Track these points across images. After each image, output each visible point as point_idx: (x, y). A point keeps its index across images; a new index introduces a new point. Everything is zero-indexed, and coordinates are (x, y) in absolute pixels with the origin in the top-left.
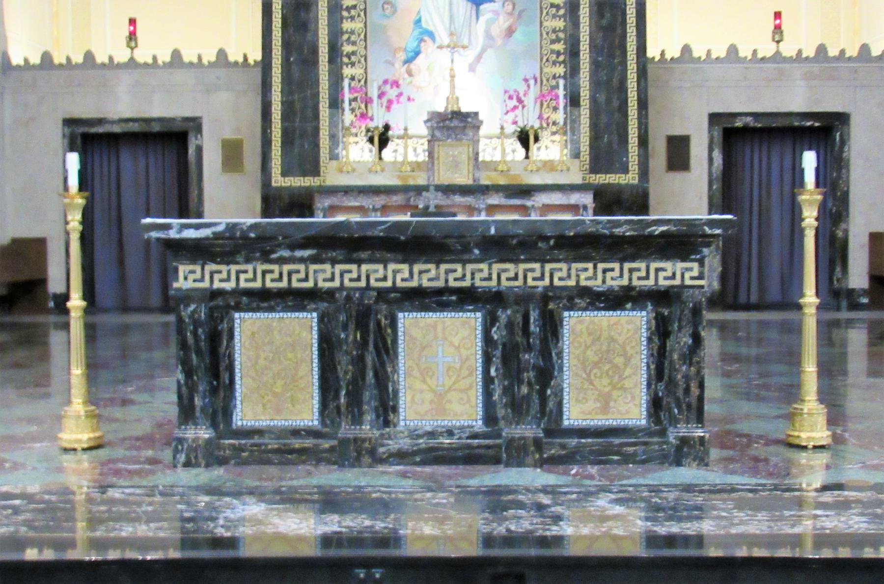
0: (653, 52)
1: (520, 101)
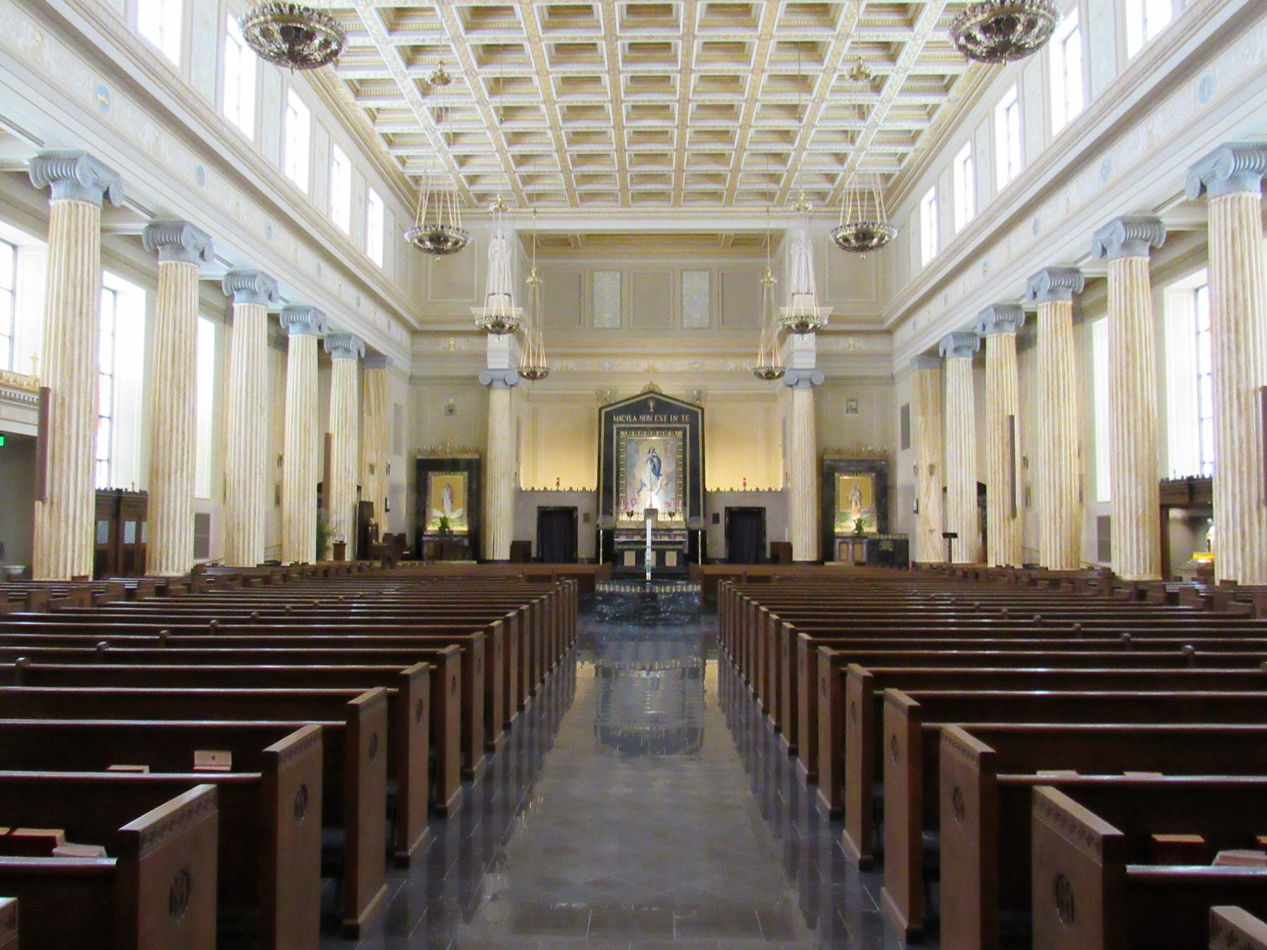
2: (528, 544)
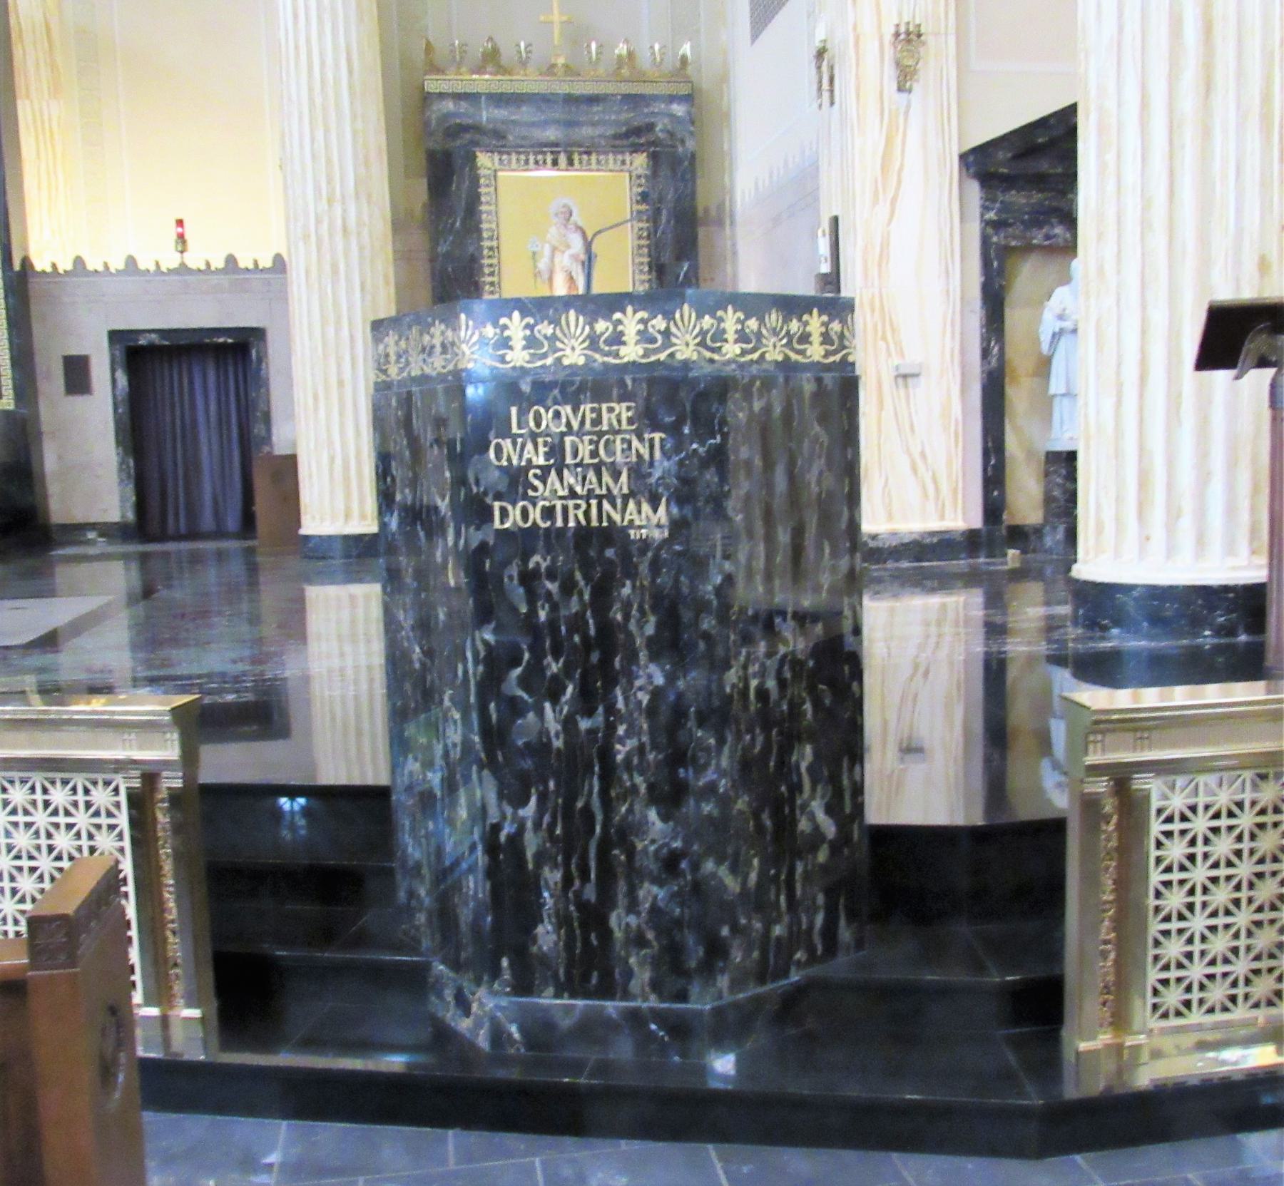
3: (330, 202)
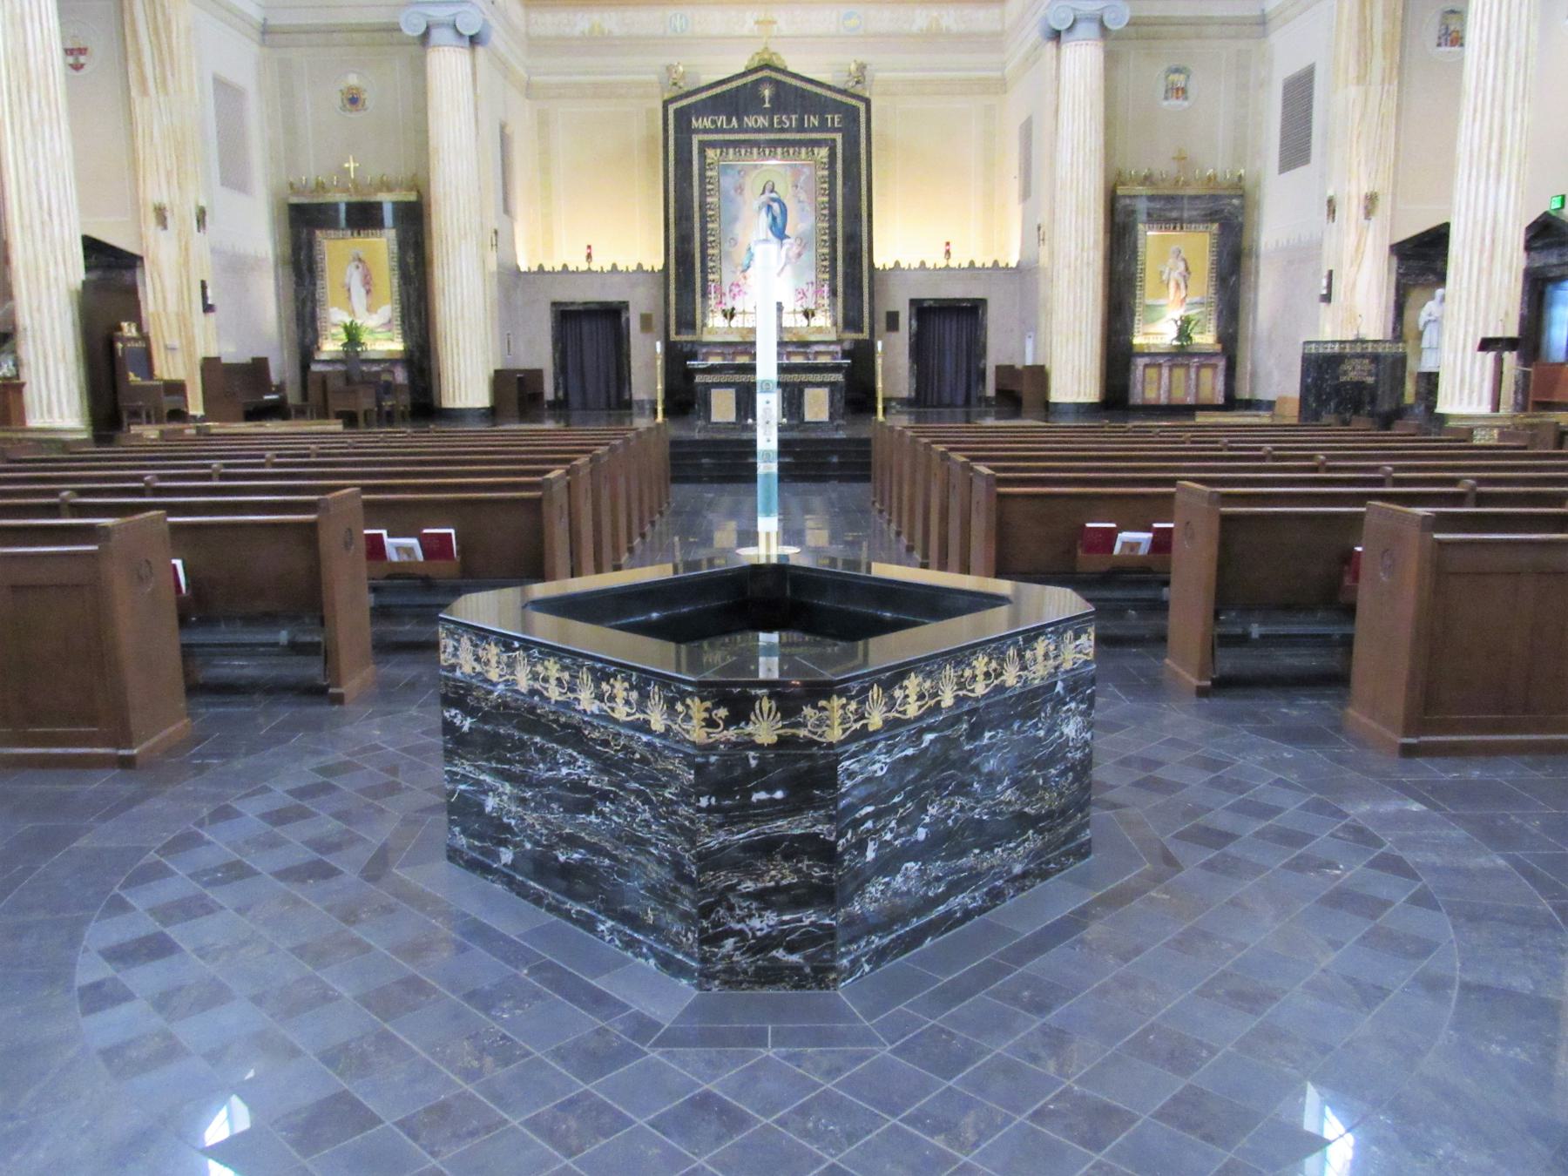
0: (878, 264)
1: (804, 294)
2: (537, 375)
3: (1082, 250)
